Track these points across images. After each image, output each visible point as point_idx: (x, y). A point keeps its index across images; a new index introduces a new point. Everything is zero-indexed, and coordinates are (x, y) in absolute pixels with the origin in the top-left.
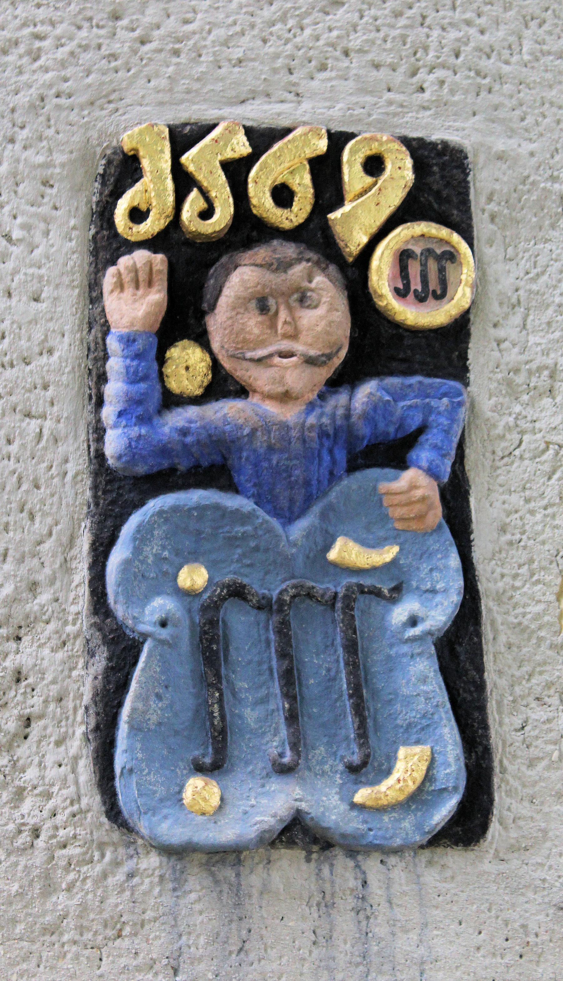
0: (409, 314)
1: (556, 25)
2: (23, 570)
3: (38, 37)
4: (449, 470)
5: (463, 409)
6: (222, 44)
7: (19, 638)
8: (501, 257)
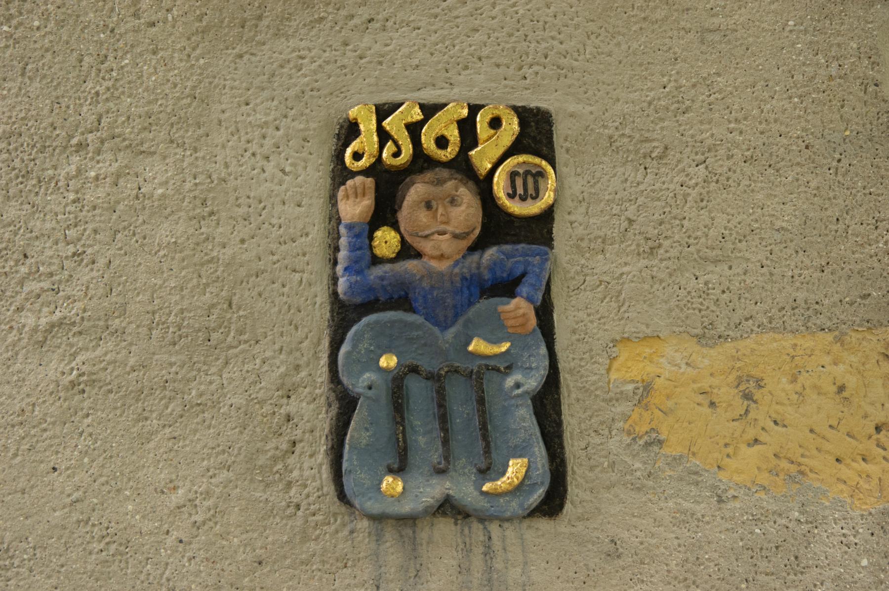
0: (516, 208)
1: (607, 37)
2: (291, 359)
3: (302, 58)
4: (540, 298)
5: (549, 263)
6: (406, 57)
7: (289, 397)
8: (573, 174)
